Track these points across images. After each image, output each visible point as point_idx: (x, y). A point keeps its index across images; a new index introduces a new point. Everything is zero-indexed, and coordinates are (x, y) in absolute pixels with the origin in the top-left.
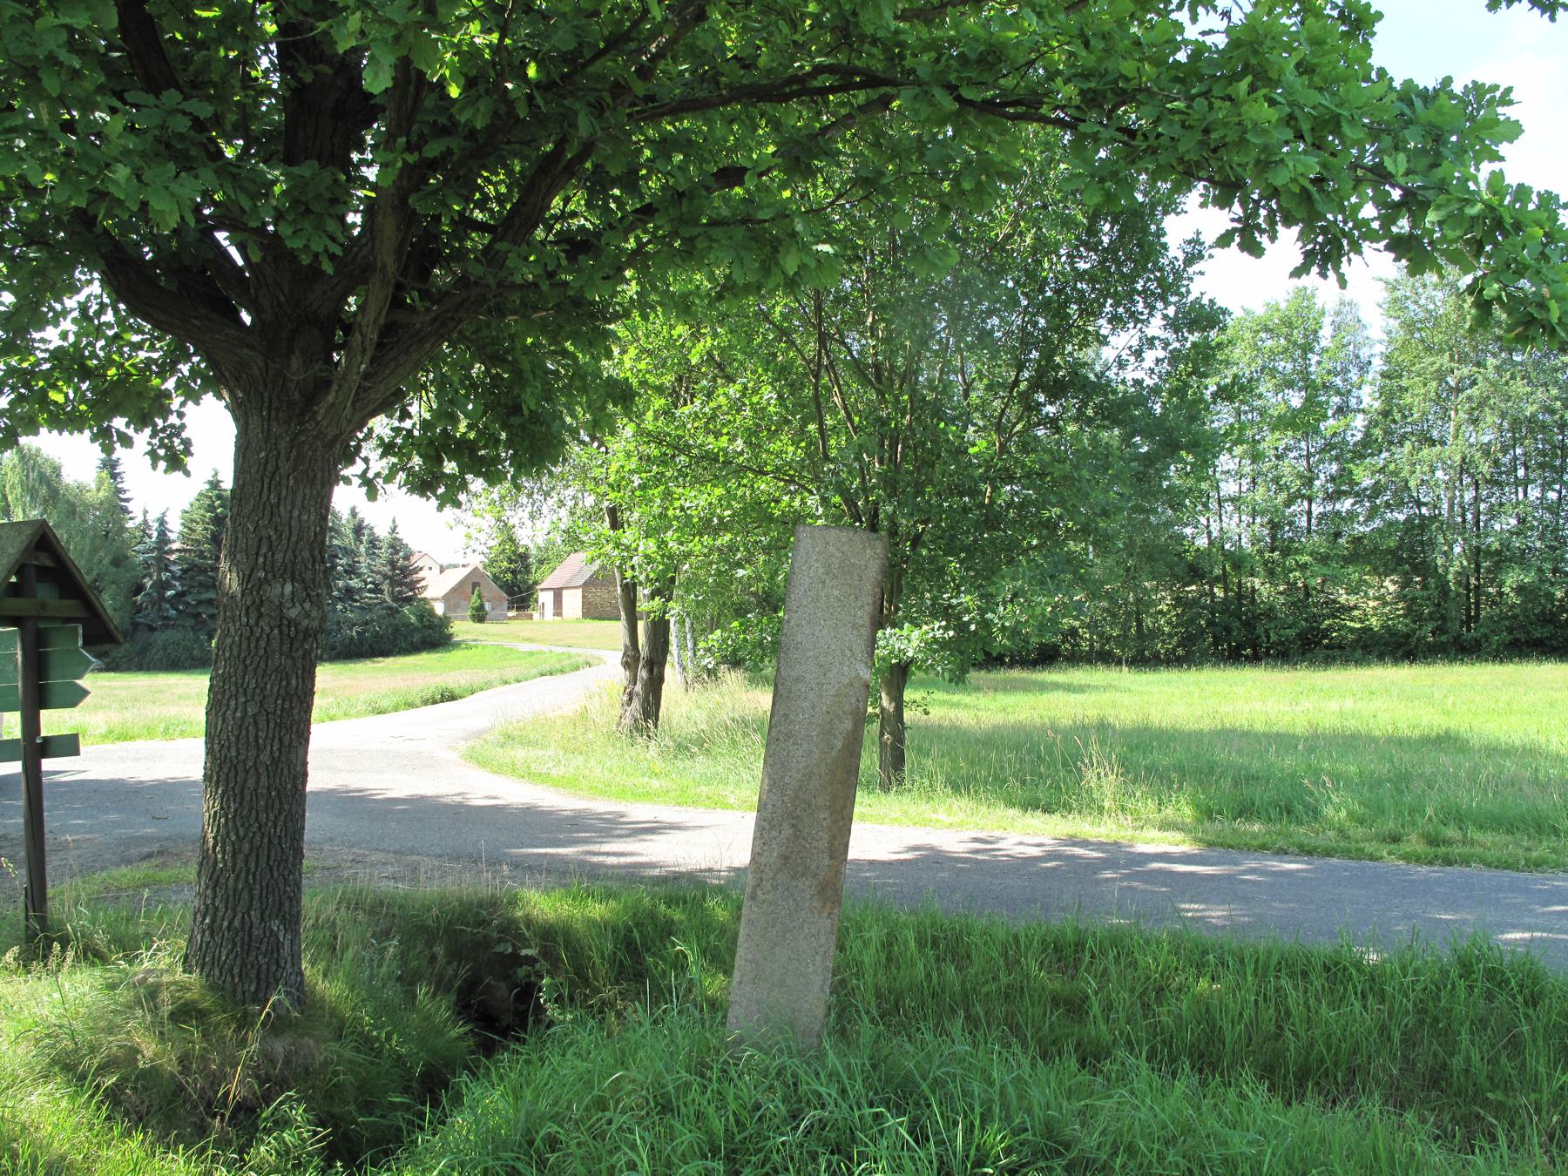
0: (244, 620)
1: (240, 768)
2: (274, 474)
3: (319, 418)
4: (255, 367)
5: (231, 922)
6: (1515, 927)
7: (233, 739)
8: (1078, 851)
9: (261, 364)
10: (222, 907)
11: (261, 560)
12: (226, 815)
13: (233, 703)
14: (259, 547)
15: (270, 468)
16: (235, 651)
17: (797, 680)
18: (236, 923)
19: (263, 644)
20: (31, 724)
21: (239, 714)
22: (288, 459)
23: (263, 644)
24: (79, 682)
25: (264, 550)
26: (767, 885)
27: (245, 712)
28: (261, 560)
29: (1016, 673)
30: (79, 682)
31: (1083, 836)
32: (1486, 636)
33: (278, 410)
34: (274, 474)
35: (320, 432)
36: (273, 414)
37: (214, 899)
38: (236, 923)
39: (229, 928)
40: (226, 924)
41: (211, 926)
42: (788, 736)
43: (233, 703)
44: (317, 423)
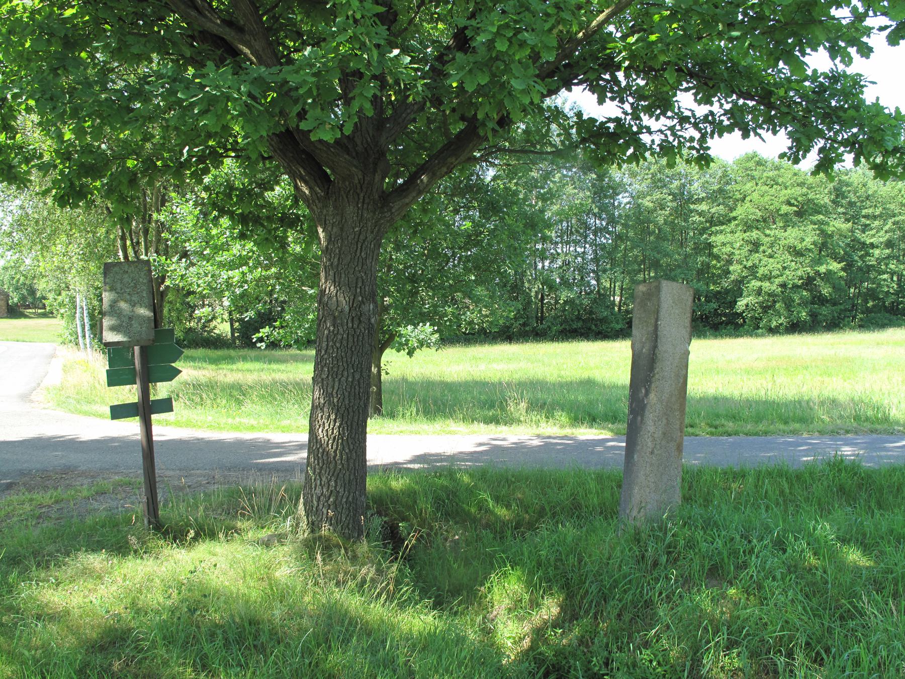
0: (350, 325)
1: (350, 410)
2: (364, 241)
3: (393, 210)
4: (356, 178)
5: (348, 498)
6: (805, 456)
7: (347, 394)
8: (552, 440)
9: (361, 177)
10: (341, 491)
11: (358, 290)
12: (342, 439)
13: (346, 373)
14: (357, 283)
15: (362, 237)
16: (345, 342)
17: (665, 352)
18: (350, 499)
19: (361, 338)
20: (145, 393)
21: (350, 379)
22: (372, 232)
23: (361, 338)
24: (173, 364)
25: (360, 284)
26: (658, 447)
27: (354, 377)
28: (358, 290)
29: (294, 351)
30: (173, 364)
31: (547, 434)
32: (549, 327)
33: (368, 204)
34: (364, 241)
35: (392, 218)
36: (365, 206)
37: (335, 487)
38: (350, 499)
39: (346, 502)
40: (344, 500)
41: (335, 502)
42: (663, 378)
43: (346, 373)
44: (392, 213)
